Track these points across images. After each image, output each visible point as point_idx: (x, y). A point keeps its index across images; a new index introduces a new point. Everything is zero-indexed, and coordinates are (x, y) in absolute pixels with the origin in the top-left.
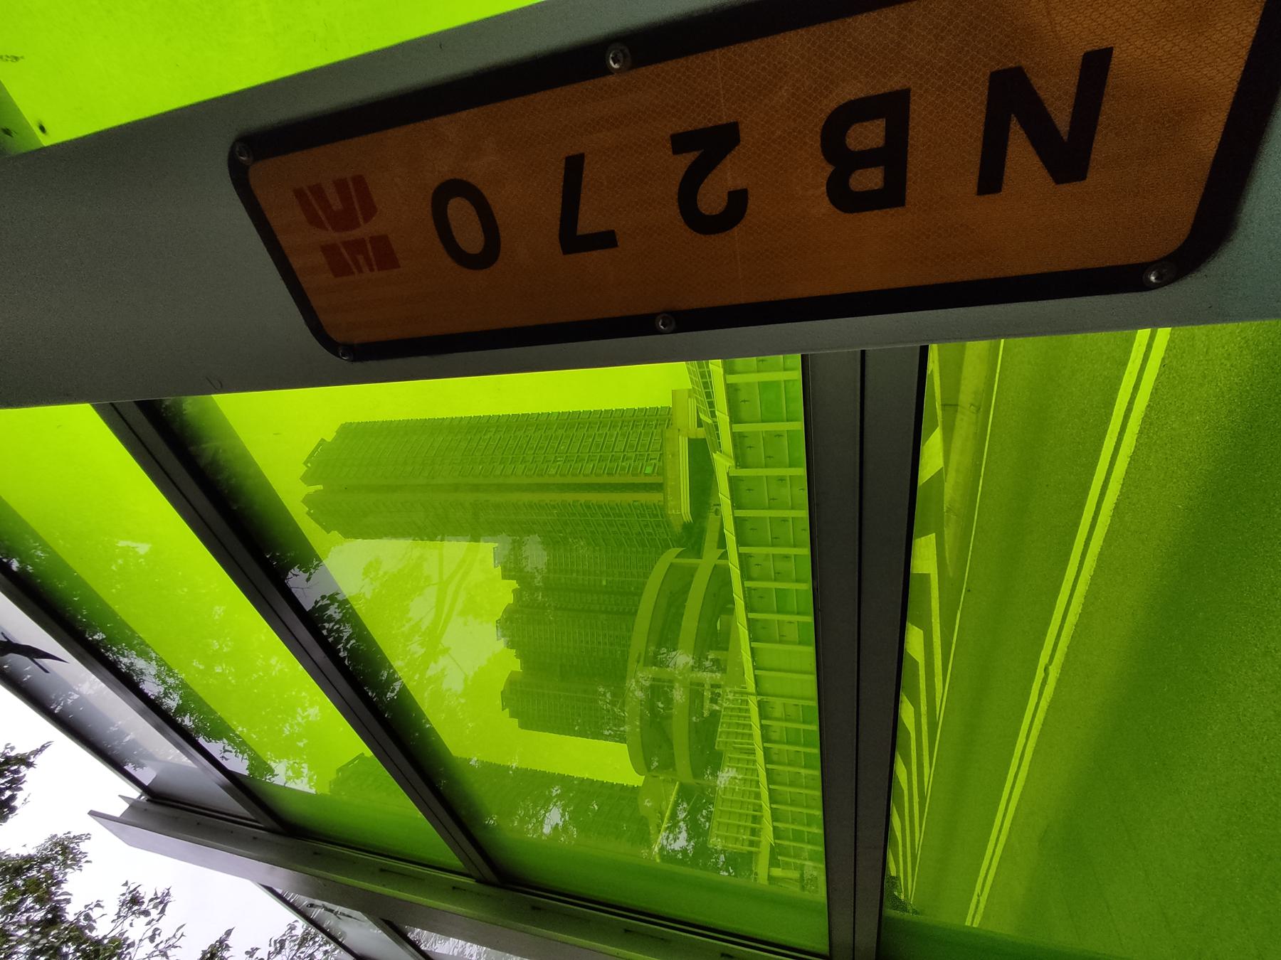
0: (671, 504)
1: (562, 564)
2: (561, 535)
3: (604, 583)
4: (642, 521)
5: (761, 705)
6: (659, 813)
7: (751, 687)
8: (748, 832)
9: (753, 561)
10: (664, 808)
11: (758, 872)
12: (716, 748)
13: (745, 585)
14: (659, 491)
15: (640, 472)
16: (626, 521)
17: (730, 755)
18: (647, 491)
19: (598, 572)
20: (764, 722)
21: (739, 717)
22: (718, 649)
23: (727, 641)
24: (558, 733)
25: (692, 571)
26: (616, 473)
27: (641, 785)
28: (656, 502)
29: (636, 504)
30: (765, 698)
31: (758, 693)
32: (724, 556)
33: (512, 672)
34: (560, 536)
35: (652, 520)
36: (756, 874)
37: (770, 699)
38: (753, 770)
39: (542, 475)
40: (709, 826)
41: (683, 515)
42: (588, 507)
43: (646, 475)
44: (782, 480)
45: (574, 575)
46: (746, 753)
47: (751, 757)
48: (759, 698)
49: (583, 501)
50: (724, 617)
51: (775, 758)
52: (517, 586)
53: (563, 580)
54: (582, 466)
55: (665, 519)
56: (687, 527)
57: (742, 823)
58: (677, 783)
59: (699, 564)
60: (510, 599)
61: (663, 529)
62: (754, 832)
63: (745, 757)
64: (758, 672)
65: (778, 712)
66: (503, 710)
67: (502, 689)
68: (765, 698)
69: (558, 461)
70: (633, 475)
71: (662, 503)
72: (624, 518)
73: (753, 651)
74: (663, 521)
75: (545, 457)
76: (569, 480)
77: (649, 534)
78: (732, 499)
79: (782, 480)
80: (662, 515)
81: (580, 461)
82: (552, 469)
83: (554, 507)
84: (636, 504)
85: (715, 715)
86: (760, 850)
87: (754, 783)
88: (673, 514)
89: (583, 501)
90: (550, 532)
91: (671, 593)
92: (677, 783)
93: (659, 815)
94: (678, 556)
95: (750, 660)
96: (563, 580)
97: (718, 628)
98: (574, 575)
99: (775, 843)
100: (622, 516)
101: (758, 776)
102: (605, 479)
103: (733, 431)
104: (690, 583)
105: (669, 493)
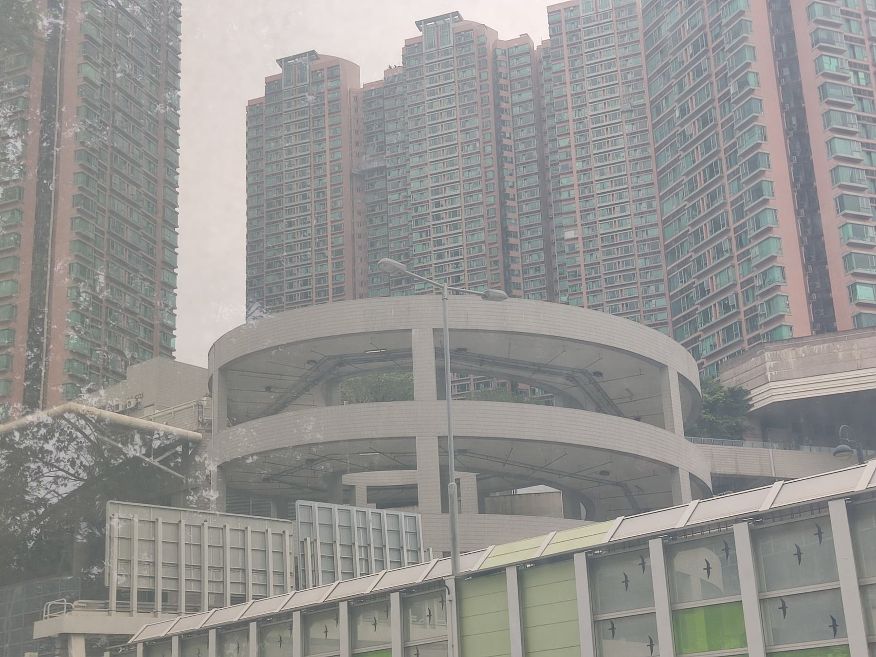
0: (789, 355)
1: (599, 133)
2: (677, 113)
3: (569, 234)
4: (737, 295)
5: (435, 587)
6: (138, 403)
7: (471, 563)
8: (145, 585)
9: (632, 570)
10: (147, 412)
11: (73, 612)
12: (299, 503)
13: (652, 543)
14: (813, 326)
15: (855, 275)
16: (730, 258)
17: (287, 533)
18: (809, 297)
19: (591, 218)
20: (395, 598)
21: (367, 547)
22: (483, 494)
23: (497, 510)
24: (249, 185)
25: (658, 419)
26: (846, 215)
27: (180, 356)
28: (787, 321)
29: (777, 274)
30: (451, 596)
31: (461, 580)
32: (702, 492)
33: (355, 68)
34: (673, 111)
35: (742, 317)
36: (69, 609)
37: (452, 610)
38: (266, 586)
39: (817, 42)
40: (252, 455)
41: (764, 388)
42: (753, 164)
43: (852, 289)
44: (834, 626)
45: (579, 166)
46: (296, 567)
47: (290, 581)
48: (451, 584)
49: (765, 149)
50: (557, 500)
51: (316, 632)
52: (537, 43)
53: (563, 142)
54: (853, 133)
55: (747, 347)
56: (738, 396)
57: (161, 572)
58: (199, 435)
59: (673, 431)
60: (507, 33)
61: (722, 346)
62: (147, 596)
63: (290, 568)
64: (512, 575)
65: (366, 631)
66: (279, 61)
67: (319, 52)
68: (451, 596)
69: (856, 73)
70: (847, 258)
71: (785, 333)
72: (736, 253)
73: (565, 558)
74: (742, 341)
75: (862, 41)
76: (814, 108)
77: (706, 315)
78: (684, 531)
79: (834, 626)
80: (757, 337)
81: (864, 126)
82: (834, 61)
83: (743, 83)
84: (777, 274)
85: (348, 496)
86: (114, 613)
87: (239, 591)
88: (764, 362)
89: (765, 149)
90: (681, 86)
91: (598, 374)
92: (199, 435)
93: (132, 405)
94: (682, 379)
95: (536, 555)
96: (563, 142)
97: (520, 491)
98: (579, 166)
99: (135, 644)
100: (740, 245)
101: (256, 598)
102: (827, 194)
103: (507, 569)
104: (619, 414)
105: (815, 348)
